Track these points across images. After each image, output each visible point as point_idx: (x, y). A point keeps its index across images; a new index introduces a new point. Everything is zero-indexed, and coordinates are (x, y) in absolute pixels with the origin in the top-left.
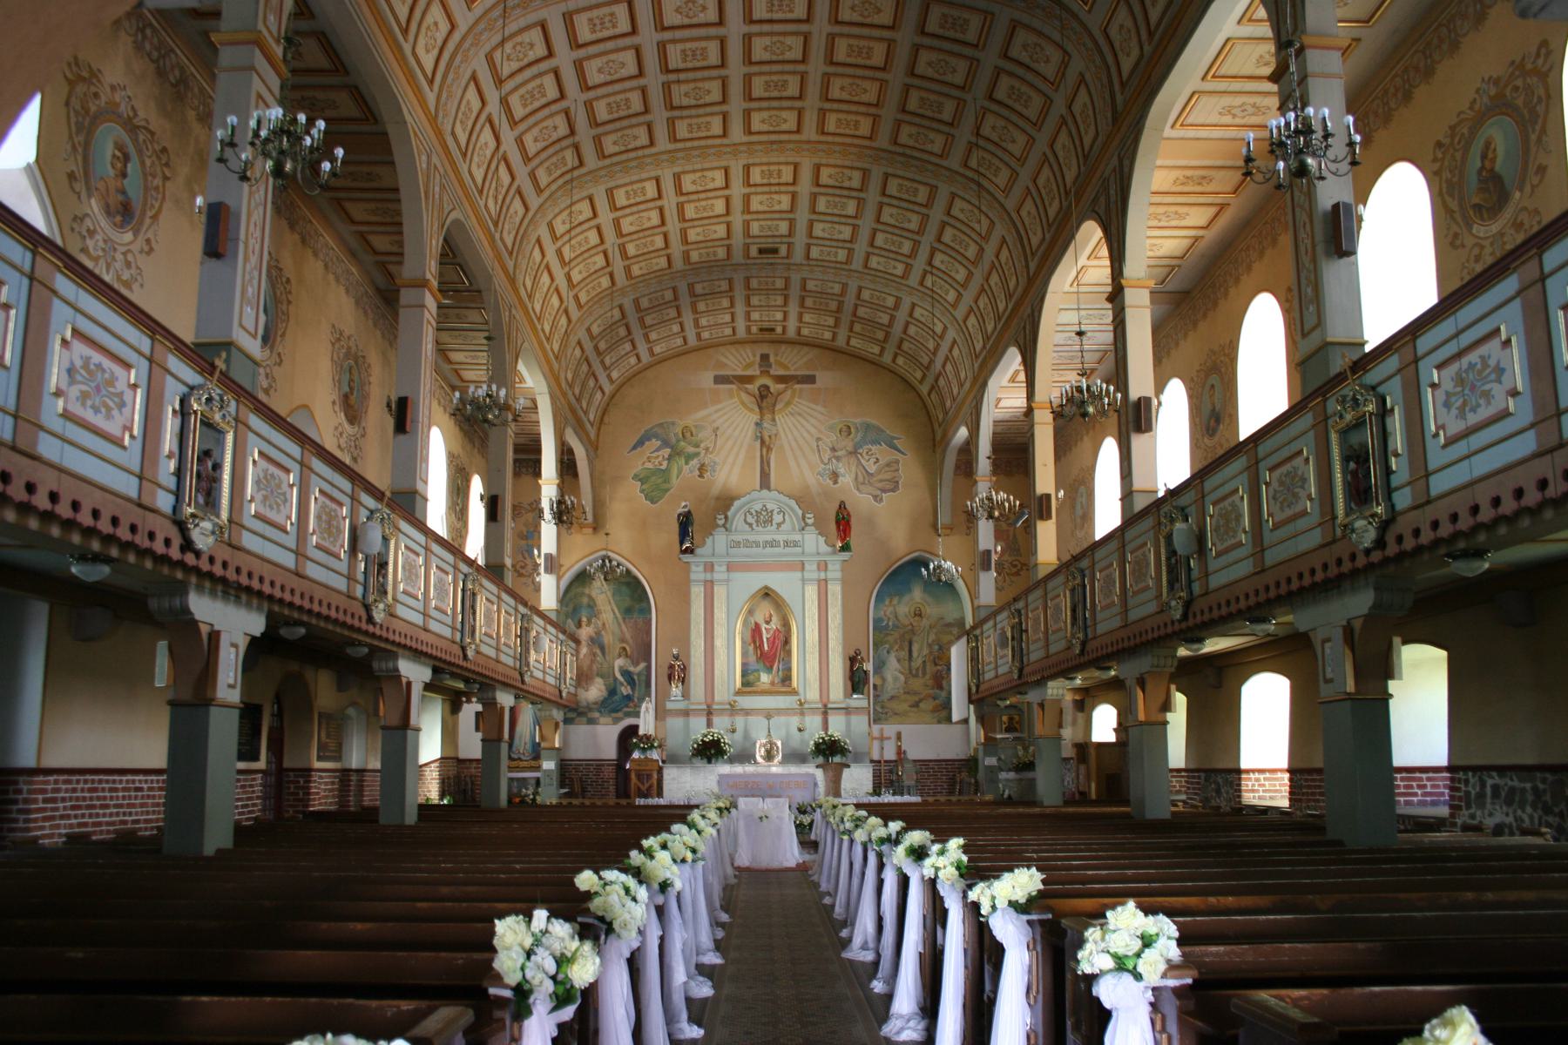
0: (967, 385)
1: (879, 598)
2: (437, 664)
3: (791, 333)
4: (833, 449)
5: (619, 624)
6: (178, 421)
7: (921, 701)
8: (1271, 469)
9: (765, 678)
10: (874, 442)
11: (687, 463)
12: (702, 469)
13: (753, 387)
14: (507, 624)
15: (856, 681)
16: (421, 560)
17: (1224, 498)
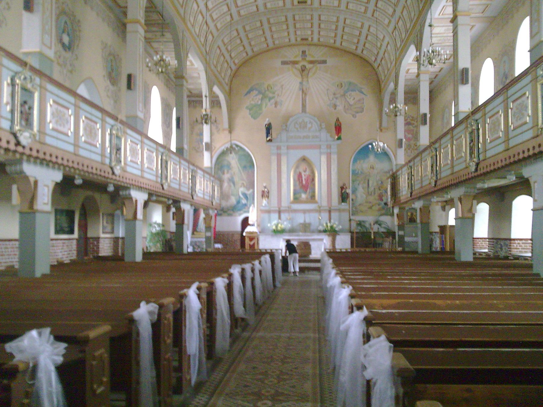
0: (394, 63)
1: (355, 161)
2: (150, 192)
3: (315, 40)
4: (334, 94)
5: (241, 173)
6: (10, 88)
7: (373, 205)
8: (513, 102)
9: (304, 196)
10: (352, 91)
11: (269, 101)
12: (276, 104)
13: (299, 66)
14: (184, 175)
15: (344, 197)
16: (139, 147)
17: (493, 116)
